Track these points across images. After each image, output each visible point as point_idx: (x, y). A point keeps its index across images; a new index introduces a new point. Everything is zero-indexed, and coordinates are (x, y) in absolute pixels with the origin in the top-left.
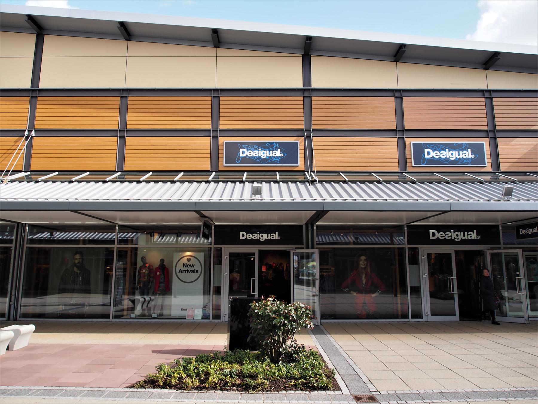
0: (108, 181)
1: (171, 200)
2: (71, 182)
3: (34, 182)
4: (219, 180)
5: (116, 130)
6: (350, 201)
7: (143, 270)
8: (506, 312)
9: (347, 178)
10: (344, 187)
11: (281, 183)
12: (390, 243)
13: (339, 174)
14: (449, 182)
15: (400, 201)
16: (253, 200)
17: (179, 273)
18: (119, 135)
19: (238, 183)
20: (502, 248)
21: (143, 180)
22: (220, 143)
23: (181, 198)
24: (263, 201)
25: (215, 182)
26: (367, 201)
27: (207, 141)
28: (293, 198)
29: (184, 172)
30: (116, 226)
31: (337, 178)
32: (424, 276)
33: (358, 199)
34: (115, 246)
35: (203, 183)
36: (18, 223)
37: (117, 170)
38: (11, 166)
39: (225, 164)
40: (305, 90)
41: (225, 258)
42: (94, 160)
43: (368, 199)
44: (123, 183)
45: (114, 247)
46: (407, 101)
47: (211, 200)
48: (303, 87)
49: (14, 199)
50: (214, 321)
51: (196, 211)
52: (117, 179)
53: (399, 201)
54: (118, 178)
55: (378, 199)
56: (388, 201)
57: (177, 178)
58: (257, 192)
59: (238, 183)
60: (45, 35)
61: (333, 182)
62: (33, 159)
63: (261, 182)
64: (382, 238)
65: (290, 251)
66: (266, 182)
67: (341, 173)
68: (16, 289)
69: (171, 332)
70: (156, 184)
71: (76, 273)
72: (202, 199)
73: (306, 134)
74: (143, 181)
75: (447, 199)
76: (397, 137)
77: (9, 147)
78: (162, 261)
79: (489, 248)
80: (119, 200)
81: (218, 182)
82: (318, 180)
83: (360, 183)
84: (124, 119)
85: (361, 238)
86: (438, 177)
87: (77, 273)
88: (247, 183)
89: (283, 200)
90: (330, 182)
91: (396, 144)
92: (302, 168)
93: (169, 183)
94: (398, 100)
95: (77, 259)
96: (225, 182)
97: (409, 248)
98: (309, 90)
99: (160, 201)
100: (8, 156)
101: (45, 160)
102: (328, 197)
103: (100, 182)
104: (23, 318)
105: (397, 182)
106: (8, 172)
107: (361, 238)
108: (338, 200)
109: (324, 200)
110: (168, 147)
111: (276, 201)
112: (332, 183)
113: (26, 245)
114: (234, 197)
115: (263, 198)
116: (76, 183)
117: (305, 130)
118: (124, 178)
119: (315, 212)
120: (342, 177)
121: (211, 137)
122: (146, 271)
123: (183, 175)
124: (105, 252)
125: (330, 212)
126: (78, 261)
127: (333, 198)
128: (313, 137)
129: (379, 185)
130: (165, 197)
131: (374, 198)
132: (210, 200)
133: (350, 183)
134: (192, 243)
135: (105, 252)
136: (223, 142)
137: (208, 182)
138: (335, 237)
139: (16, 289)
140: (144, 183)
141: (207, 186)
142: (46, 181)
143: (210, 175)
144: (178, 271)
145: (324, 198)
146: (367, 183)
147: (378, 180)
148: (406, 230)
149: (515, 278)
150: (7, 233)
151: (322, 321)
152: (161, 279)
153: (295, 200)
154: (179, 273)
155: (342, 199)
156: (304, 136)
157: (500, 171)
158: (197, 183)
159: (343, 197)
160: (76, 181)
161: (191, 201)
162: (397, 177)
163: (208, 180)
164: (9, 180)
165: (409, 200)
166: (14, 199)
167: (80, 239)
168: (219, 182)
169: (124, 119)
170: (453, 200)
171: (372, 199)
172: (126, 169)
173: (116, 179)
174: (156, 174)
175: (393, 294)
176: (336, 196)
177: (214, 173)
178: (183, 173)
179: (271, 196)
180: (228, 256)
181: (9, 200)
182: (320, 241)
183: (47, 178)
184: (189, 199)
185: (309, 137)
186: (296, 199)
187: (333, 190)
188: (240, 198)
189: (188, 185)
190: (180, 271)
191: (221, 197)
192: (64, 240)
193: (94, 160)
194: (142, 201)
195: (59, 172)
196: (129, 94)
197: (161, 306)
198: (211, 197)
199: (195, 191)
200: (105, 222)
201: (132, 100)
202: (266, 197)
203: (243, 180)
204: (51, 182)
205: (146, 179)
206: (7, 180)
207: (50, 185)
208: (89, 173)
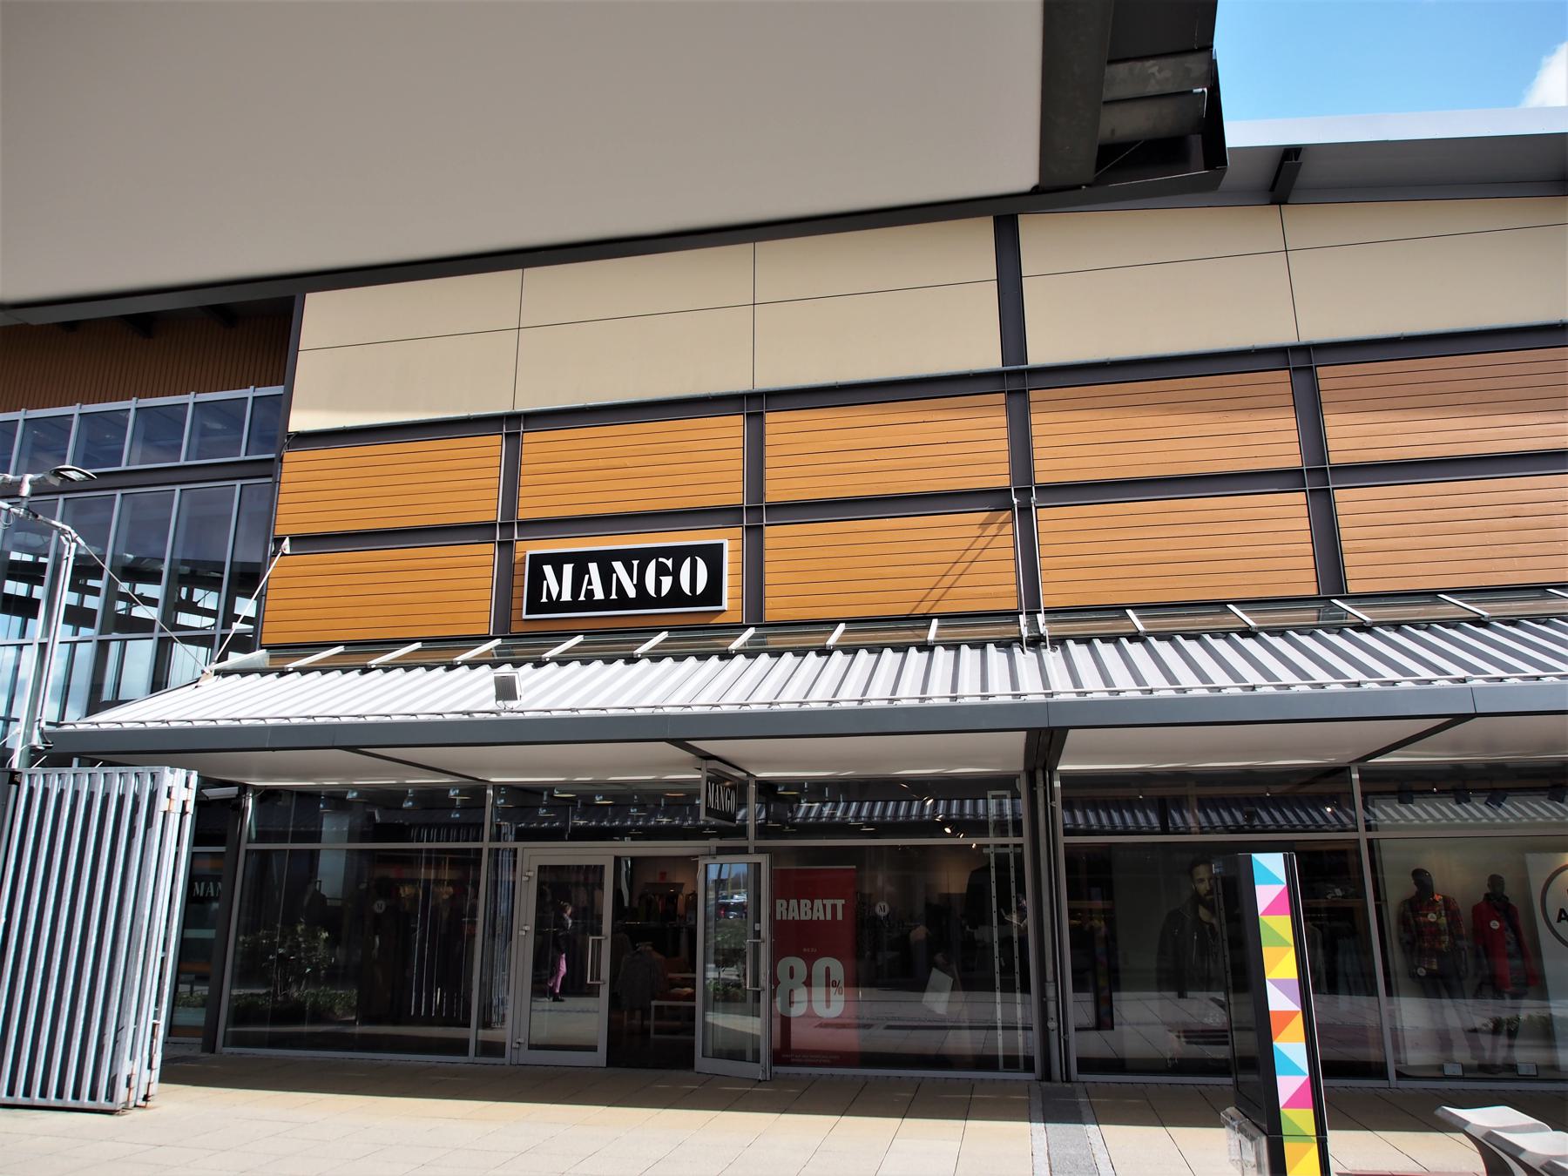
0: (459, 663)
1: (689, 710)
2: (451, 667)
3: (444, 667)
5: (737, 510)
7: (1426, 916)
8: (1386, 1059)
9: (1145, 626)
10: (1303, 643)
13: (1224, 609)
14: (1487, 620)
16: (895, 703)
17: (1559, 921)
18: (498, 539)
19: (913, 650)
20: (751, 850)
21: (642, 654)
22: (518, 556)
23: (775, 698)
24: (1055, 697)
26: (1259, 690)
27: (1293, 506)
28: (1083, 688)
29: (848, 621)
30: (1352, 769)
31: (1223, 622)
33: (1261, 686)
34: (486, 845)
35: (812, 655)
37: (491, 634)
39: (527, 614)
40: (1009, 373)
41: (525, 879)
42: (1241, 565)
43: (1329, 684)
45: (1366, 841)
46: (1328, 376)
48: (1003, 366)
49: (232, 719)
50: (478, 1060)
52: (493, 656)
53: (1365, 687)
54: (495, 654)
55: (1262, 684)
56: (1259, 690)
57: (736, 645)
58: (506, 690)
59: (913, 650)
60: (1019, 216)
62: (1047, 574)
63: (1426, 626)
64: (1312, 813)
65: (697, 861)
66: (972, 646)
67: (1230, 606)
68: (1056, 980)
69: (730, 1106)
70: (677, 664)
71: (1208, 926)
72: (807, 703)
73: (1015, 501)
74: (644, 655)
76: (1305, 491)
77: (966, 543)
78: (1495, 881)
79: (714, 850)
80: (313, 717)
82: (1049, 636)
83: (1357, 632)
84: (1313, 435)
85: (1264, 815)
86: (1483, 605)
87: (1212, 926)
88: (939, 650)
89: (1052, 695)
91: (1304, 511)
92: (737, 617)
93: (714, 660)
94: (1303, 378)
95: (1202, 880)
96: (876, 649)
97: (479, 851)
98: (1022, 372)
100: (967, 568)
101: (1082, 574)
104: (233, 1045)
105: (1310, 631)
107: (1264, 815)
108: (1127, 692)
109: (1151, 691)
110: (1177, 531)
111: (1030, 699)
112: (1179, 638)
113: (1063, 840)
115: (1054, 689)
116: (553, 666)
117: (1015, 489)
118: (1342, 618)
120: (1236, 617)
121: (742, 526)
122: (1439, 916)
123: (845, 632)
126: (1208, 888)
127: (1180, 684)
128: (1036, 508)
129: (1364, 637)
130: (702, 699)
132: (801, 703)
133: (1263, 635)
136: (525, 556)
137: (825, 652)
138: (1118, 814)
139: (1056, 980)
140: (645, 663)
142: (304, 671)
143: (832, 632)
144: (1553, 916)
145: (1251, 684)
146: (1292, 633)
147: (1358, 621)
148: (1057, 788)
150: (635, 810)
151: (775, 1069)
152: (1509, 943)
154: (1559, 921)
156: (1011, 508)
157: (1347, 593)
159: (1214, 680)
160: (464, 663)
161: (808, 706)
162: (1315, 614)
163: (825, 646)
165: (1366, 682)
166: (232, 719)
168: (960, 645)
169: (1313, 435)
170: (1516, 677)
171: (1341, 683)
172: (769, 616)
173: (492, 658)
175: (1086, 991)
176: (1220, 678)
177: (844, 624)
178: (753, 628)
179: (984, 686)
180: (534, 874)
181: (295, 721)
182: (1229, 824)
183: (393, 659)
184: (771, 704)
185: (1025, 510)
186: (1158, 690)
188: (952, 692)
189: (743, 663)
190: (1563, 916)
191: (864, 693)
193: (1241, 565)
194: (639, 711)
195: (347, 644)
196: (747, 407)
197: (1025, 1032)
198: (834, 696)
199: (788, 680)
200: (453, 777)
201: (1328, 376)
204: (578, 663)
205: (651, 649)
208: (420, 643)
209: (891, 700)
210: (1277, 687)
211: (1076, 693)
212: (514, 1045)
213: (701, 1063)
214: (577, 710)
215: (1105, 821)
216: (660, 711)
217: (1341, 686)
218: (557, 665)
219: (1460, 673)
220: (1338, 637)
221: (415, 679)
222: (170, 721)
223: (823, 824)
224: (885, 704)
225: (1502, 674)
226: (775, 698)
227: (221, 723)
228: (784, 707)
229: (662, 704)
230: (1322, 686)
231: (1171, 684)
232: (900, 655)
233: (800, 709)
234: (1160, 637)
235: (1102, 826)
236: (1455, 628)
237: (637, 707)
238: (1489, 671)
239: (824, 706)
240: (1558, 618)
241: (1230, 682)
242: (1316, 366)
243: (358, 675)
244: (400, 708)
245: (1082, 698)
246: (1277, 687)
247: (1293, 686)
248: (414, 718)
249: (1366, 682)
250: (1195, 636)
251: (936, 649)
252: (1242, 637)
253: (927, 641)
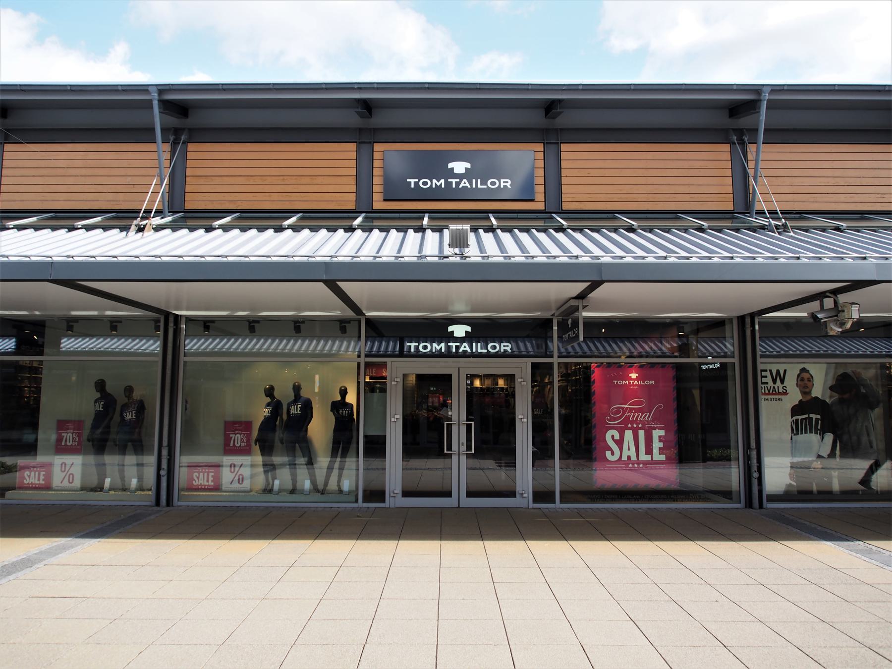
4: (547, 226)
6: (565, 260)
11: (429, 232)
12: (668, 354)
15: (629, 259)
16: (400, 259)
19: (411, 231)
23: (336, 253)
25: (364, 230)
28: (486, 254)
32: (393, 420)
36: (167, 315)
38: (152, 201)
43: (603, 257)
44: (228, 231)
47: (355, 259)
49: (66, 257)
51: (326, 282)
53: (581, 260)
59: (411, 231)
61: (536, 229)
69: (236, 536)
70: (243, 233)
72: (336, 257)
75: (663, 254)
81: (370, 230)
83: (592, 232)
90: (477, 229)
96: (386, 230)
99: (313, 259)
102: (519, 252)
103: (267, 229)
106: (148, 211)
114: (365, 251)
116: (220, 231)
119: (589, 284)
124: (838, 459)
125: (606, 284)
130: (303, 252)
131: (572, 253)
132: (375, 257)
133: (569, 231)
134: (222, 350)
135: (838, 459)
138: (523, 344)
141: (348, 236)
142: (20, 228)
147: (559, 224)
149: (472, 421)
153: (490, 259)
155: (568, 257)
158: (328, 231)
161: (336, 259)
164: (154, 226)
165: (582, 256)
166: (66, 257)
167: (237, 351)
174: (307, 215)
182: (530, 350)
187: (549, 239)
191: (378, 252)
192: (101, 352)
202: (473, 253)
203: (422, 225)
206: (151, 225)
207: (168, 235)
209: (397, 257)
210: (570, 257)
211: (482, 257)
212: (392, 495)
213: (766, 504)
214: (226, 257)
215: (523, 349)
216: (291, 259)
217: (653, 258)
218: (222, 232)
219: (662, 253)
220: (579, 234)
221: (164, 237)
222: (162, 256)
223: (231, 352)
224: (392, 259)
225: (644, 254)
226: (336, 253)
227: (34, 259)
228: (363, 259)
229: (292, 255)
230: (597, 257)
231: (544, 253)
232: (402, 234)
233: (352, 261)
234: (504, 230)
235: (521, 352)
236: (668, 232)
237: (250, 256)
238: (679, 252)
239: (370, 259)
240: (676, 229)
241: (561, 253)
242: (561, 143)
243: (65, 233)
244: (215, 249)
245: (508, 261)
246: (570, 257)
247: (558, 257)
248: (181, 259)
249: (582, 256)
250: (526, 230)
251: (427, 230)
252: (520, 232)
253: (352, 225)
